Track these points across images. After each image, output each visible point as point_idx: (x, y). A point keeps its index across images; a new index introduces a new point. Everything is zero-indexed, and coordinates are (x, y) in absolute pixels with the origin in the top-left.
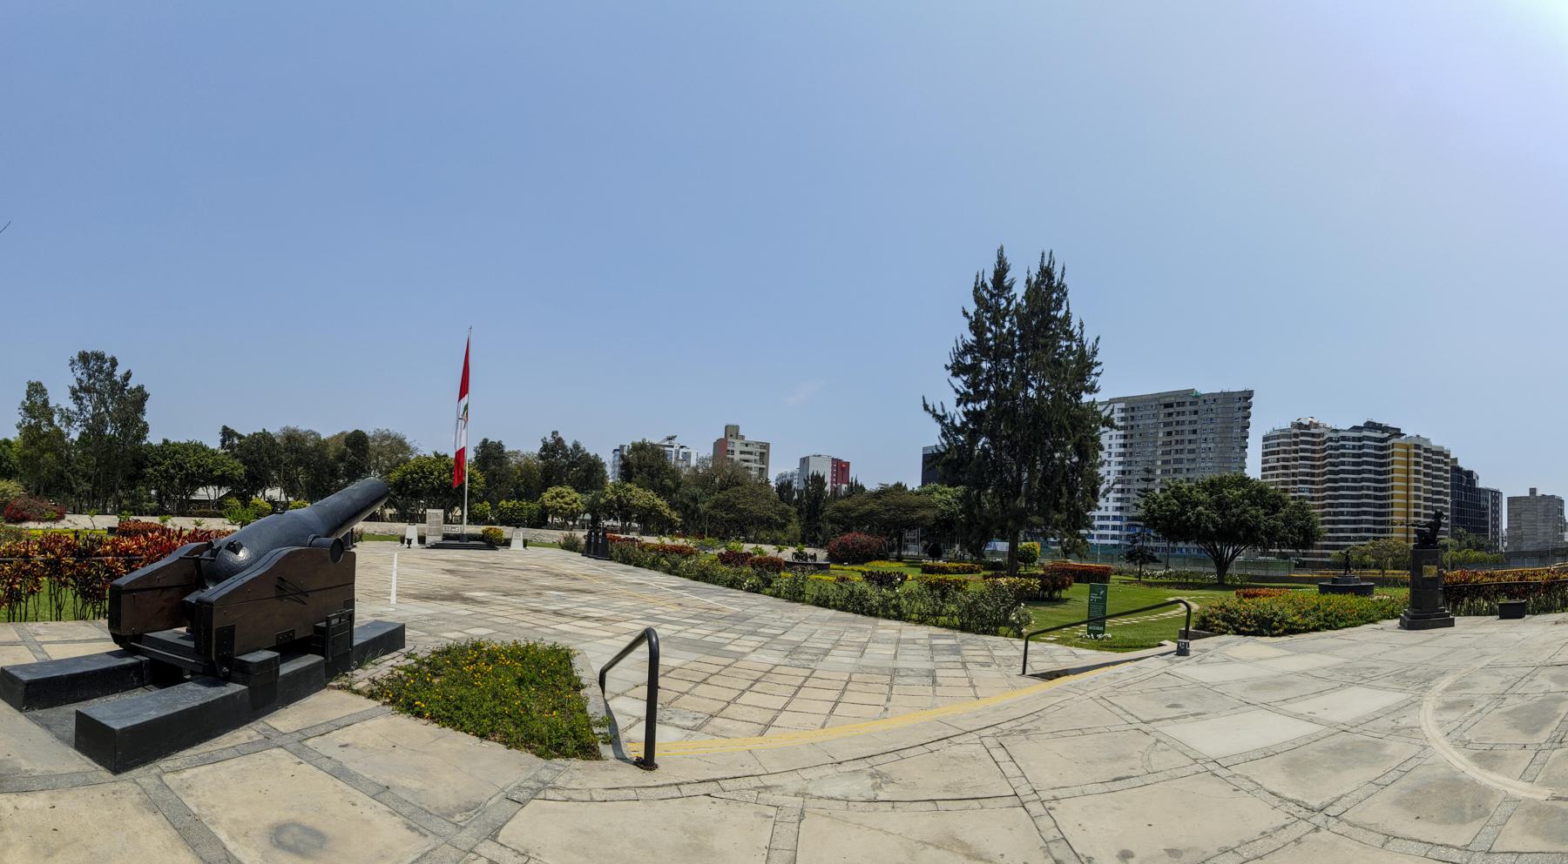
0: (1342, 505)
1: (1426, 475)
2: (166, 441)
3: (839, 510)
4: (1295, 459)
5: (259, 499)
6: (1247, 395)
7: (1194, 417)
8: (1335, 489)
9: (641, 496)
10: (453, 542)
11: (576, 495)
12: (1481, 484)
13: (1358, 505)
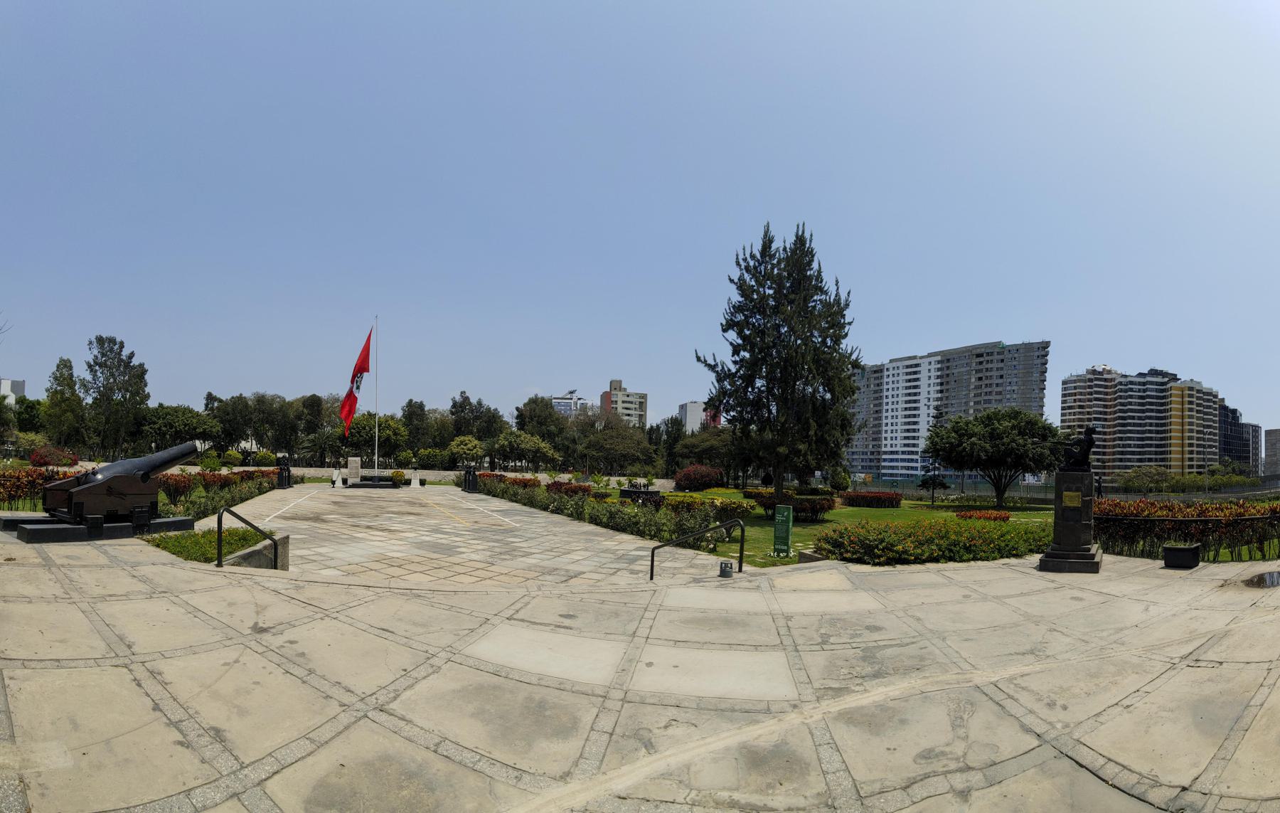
0: (1130, 439)
1: (1198, 412)
2: (161, 405)
3: (686, 446)
4: (1090, 400)
5: (232, 452)
6: (1045, 345)
7: (1001, 365)
8: (1124, 425)
9: (530, 441)
10: (368, 482)
11: (476, 442)
12: (1244, 420)
13: (1142, 439)
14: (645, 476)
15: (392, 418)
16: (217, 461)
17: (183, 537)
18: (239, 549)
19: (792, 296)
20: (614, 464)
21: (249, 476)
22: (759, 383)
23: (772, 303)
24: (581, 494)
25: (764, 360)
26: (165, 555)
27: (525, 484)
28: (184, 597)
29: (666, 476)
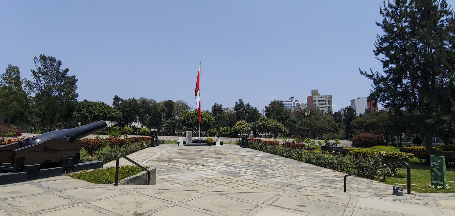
2: (85, 101)
3: (357, 122)
5: (128, 127)
11: (247, 124)
14: (334, 139)
15: (207, 112)
16: (119, 132)
17: (95, 172)
18: (128, 176)
19: (424, 23)
20: (317, 133)
21: (136, 140)
22: (405, 81)
23: (408, 30)
24: (300, 148)
25: (407, 67)
26: (83, 183)
27: (271, 143)
28: (94, 203)
29: (346, 138)
